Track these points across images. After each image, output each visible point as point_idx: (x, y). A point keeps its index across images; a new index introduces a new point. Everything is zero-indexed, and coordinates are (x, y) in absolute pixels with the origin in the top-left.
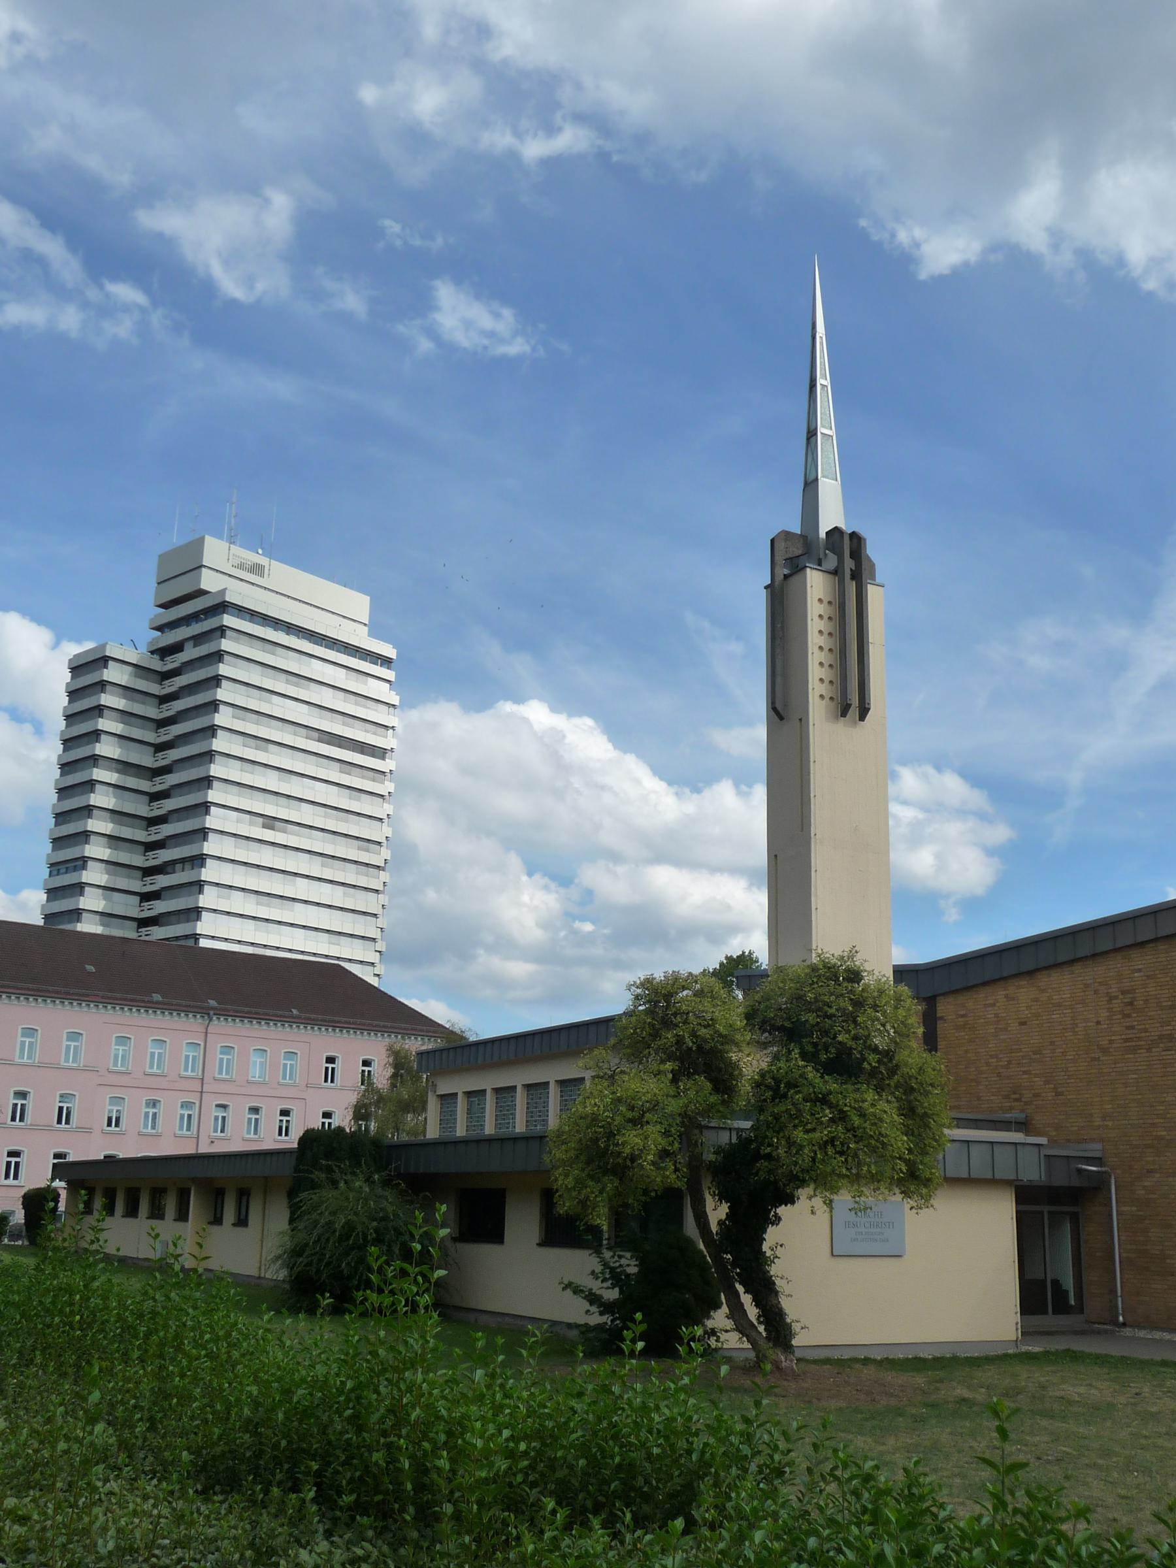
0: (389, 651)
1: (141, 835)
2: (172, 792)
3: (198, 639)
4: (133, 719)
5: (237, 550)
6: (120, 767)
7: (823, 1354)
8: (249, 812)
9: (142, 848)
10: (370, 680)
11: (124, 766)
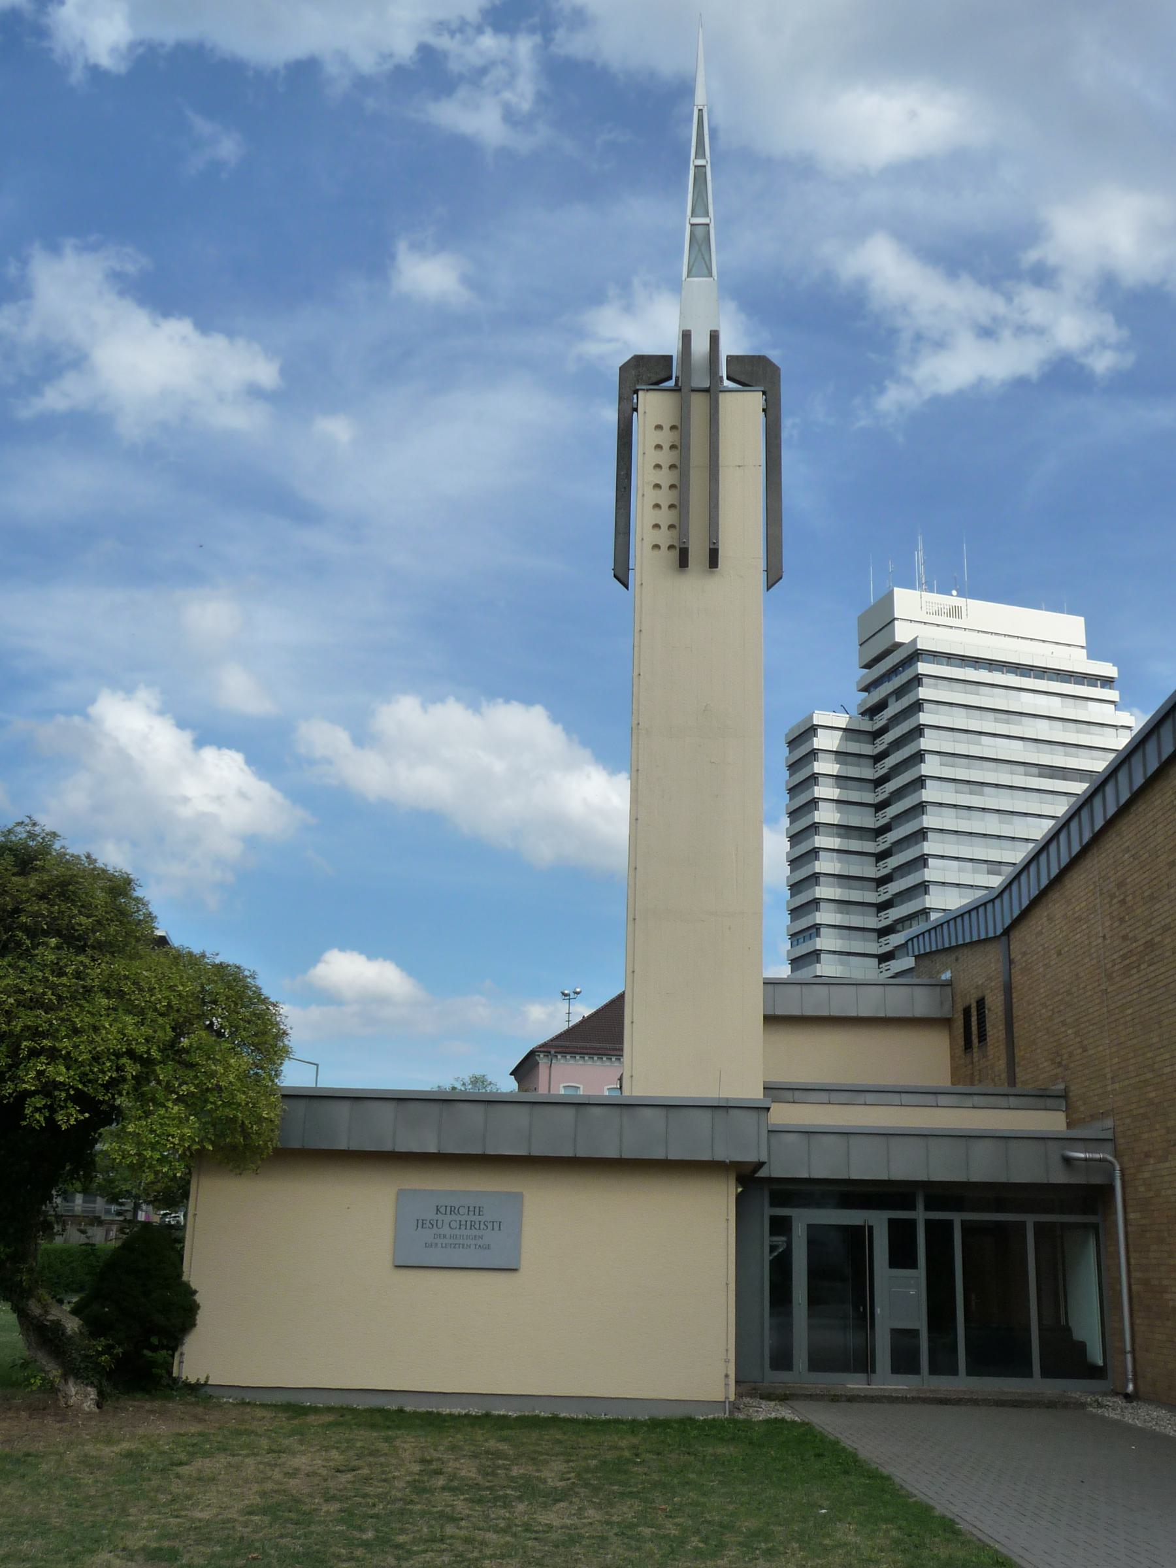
0: (1108, 669)
1: (871, 897)
2: (894, 850)
3: (899, 693)
4: (850, 783)
5: (929, 596)
6: (842, 831)
7: (334, 1402)
8: (971, 860)
9: (874, 910)
10: (1090, 703)
11: (845, 830)
